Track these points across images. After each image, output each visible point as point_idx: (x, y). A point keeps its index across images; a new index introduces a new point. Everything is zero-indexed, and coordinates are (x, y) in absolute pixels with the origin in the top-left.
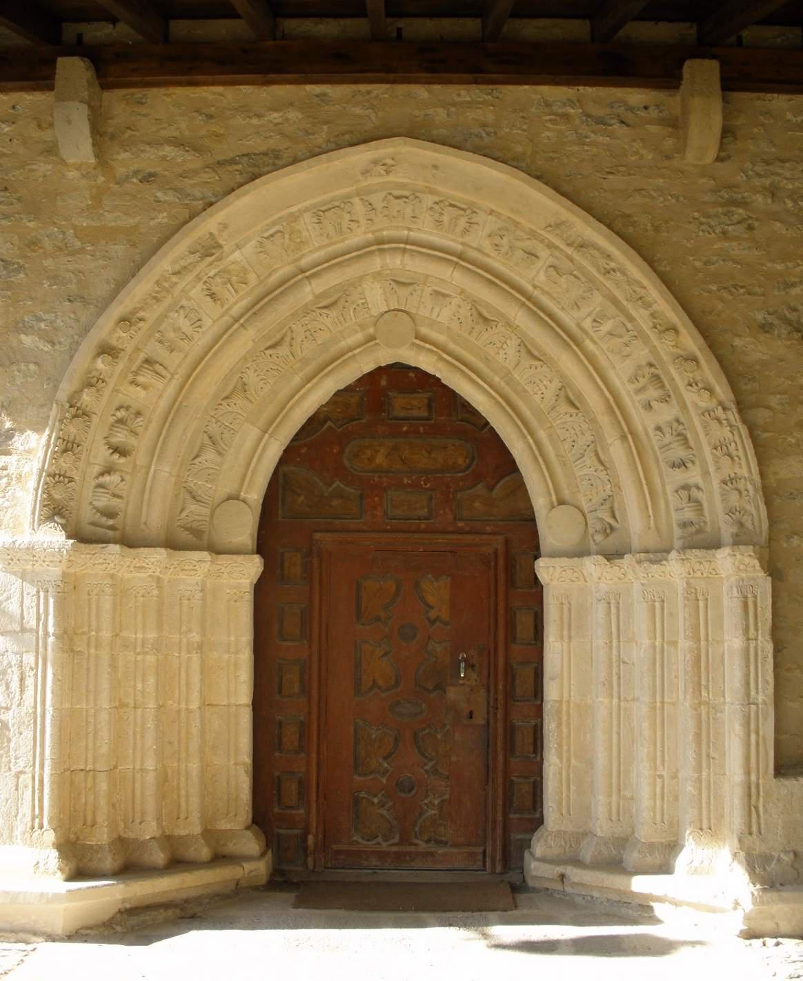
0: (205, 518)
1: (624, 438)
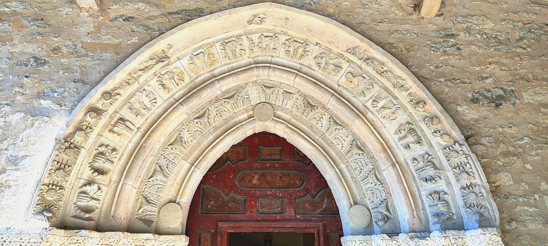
0: (154, 214)
1: (394, 165)
